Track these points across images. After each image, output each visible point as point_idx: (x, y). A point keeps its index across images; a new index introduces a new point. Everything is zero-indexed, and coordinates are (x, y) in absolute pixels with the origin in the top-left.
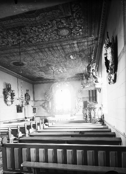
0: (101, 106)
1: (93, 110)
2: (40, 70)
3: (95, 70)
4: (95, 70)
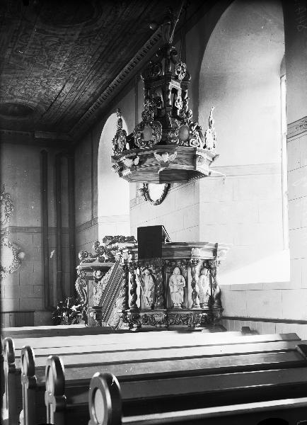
1: (177, 270)
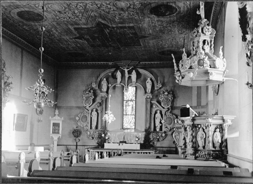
0: (220, 122)
2: (78, 35)
3: (209, 42)
4: (209, 42)
